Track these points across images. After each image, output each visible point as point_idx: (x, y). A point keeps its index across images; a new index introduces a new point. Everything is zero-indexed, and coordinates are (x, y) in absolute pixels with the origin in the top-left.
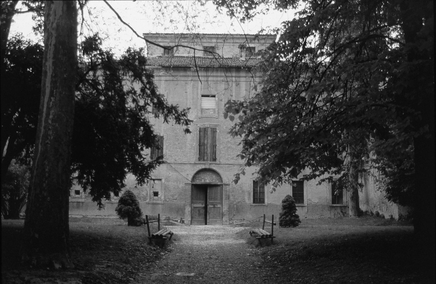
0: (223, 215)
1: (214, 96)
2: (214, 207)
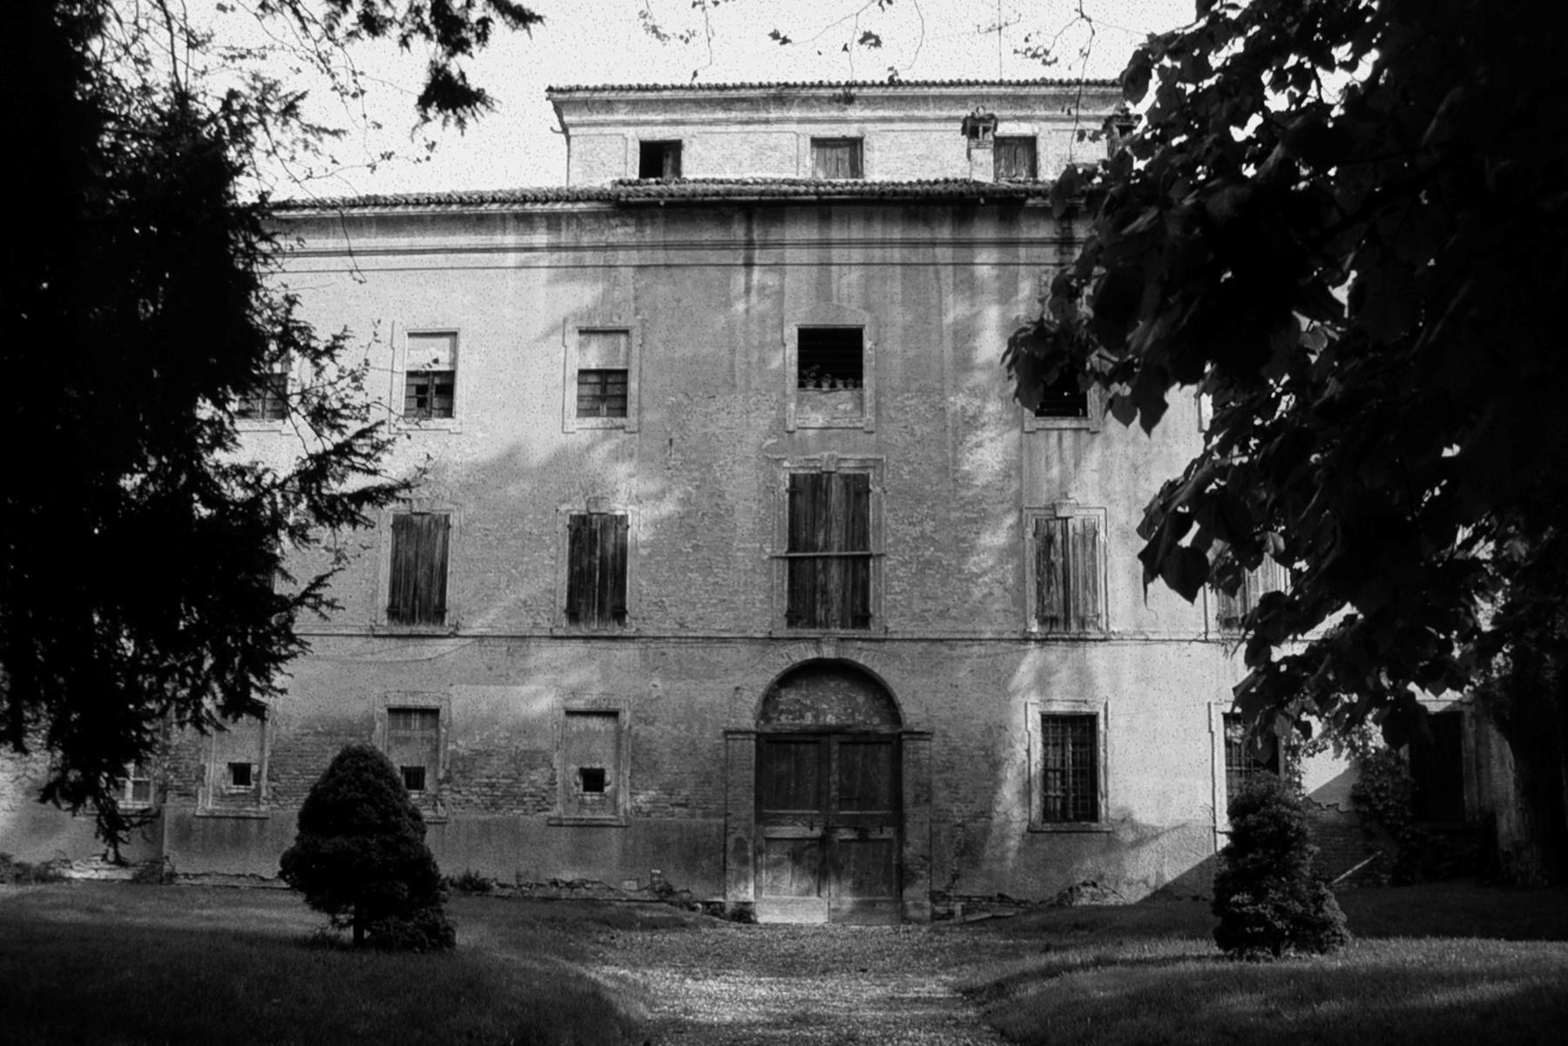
0: (902, 877)
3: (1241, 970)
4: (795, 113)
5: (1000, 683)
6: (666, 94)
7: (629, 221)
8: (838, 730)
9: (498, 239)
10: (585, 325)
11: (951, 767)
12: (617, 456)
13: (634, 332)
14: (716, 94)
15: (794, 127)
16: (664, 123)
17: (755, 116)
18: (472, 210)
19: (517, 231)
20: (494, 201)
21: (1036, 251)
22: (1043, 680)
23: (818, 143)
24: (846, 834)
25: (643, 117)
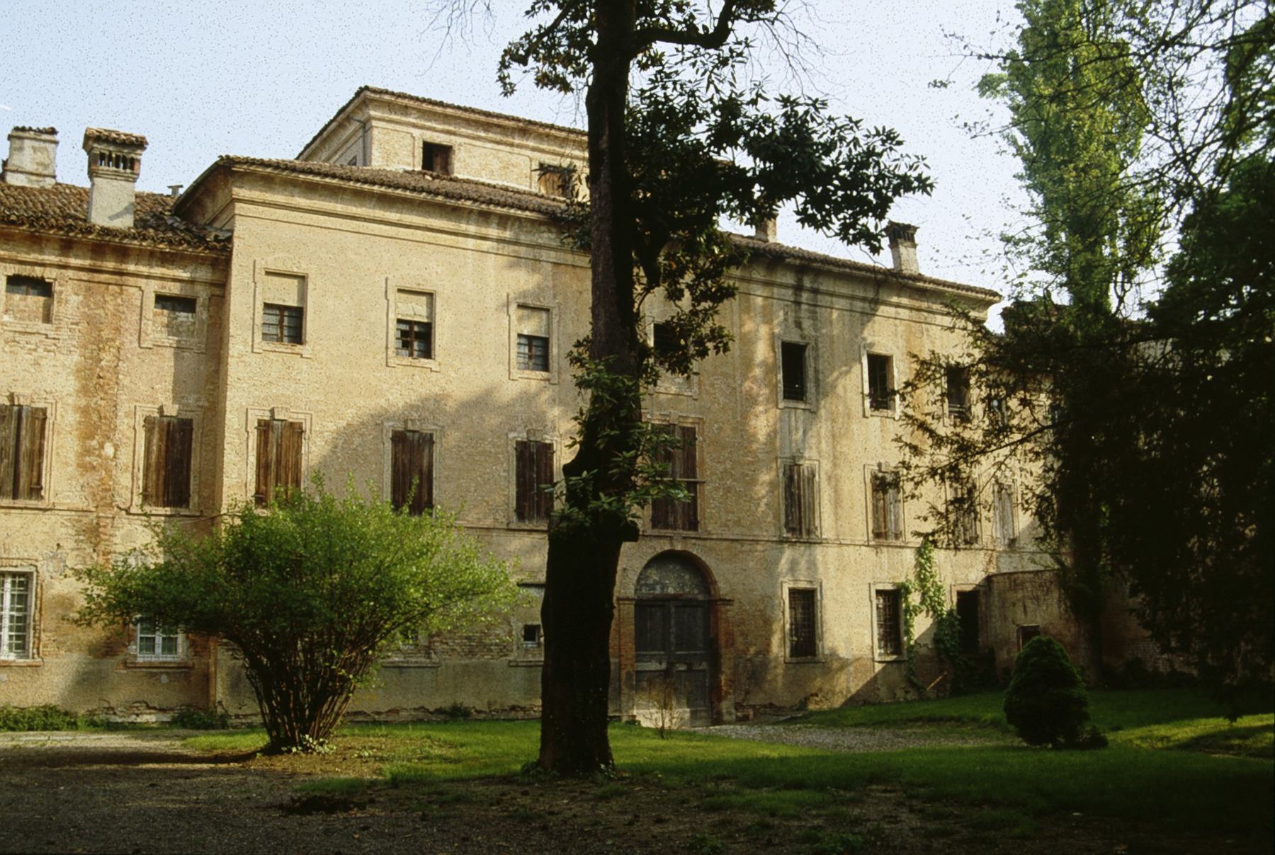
3: (1233, 718)
4: (531, 143)
5: (770, 567)
6: (449, 111)
7: (553, 230)
8: (675, 598)
9: (463, 227)
10: (521, 301)
11: (743, 622)
12: (553, 401)
13: (555, 311)
14: (483, 118)
15: (528, 153)
16: (443, 131)
17: (505, 139)
18: (453, 202)
19: (478, 224)
21: (783, 291)
22: (793, 567)
23: (544, 169)
24: (683, 668)
25: (428, 124)
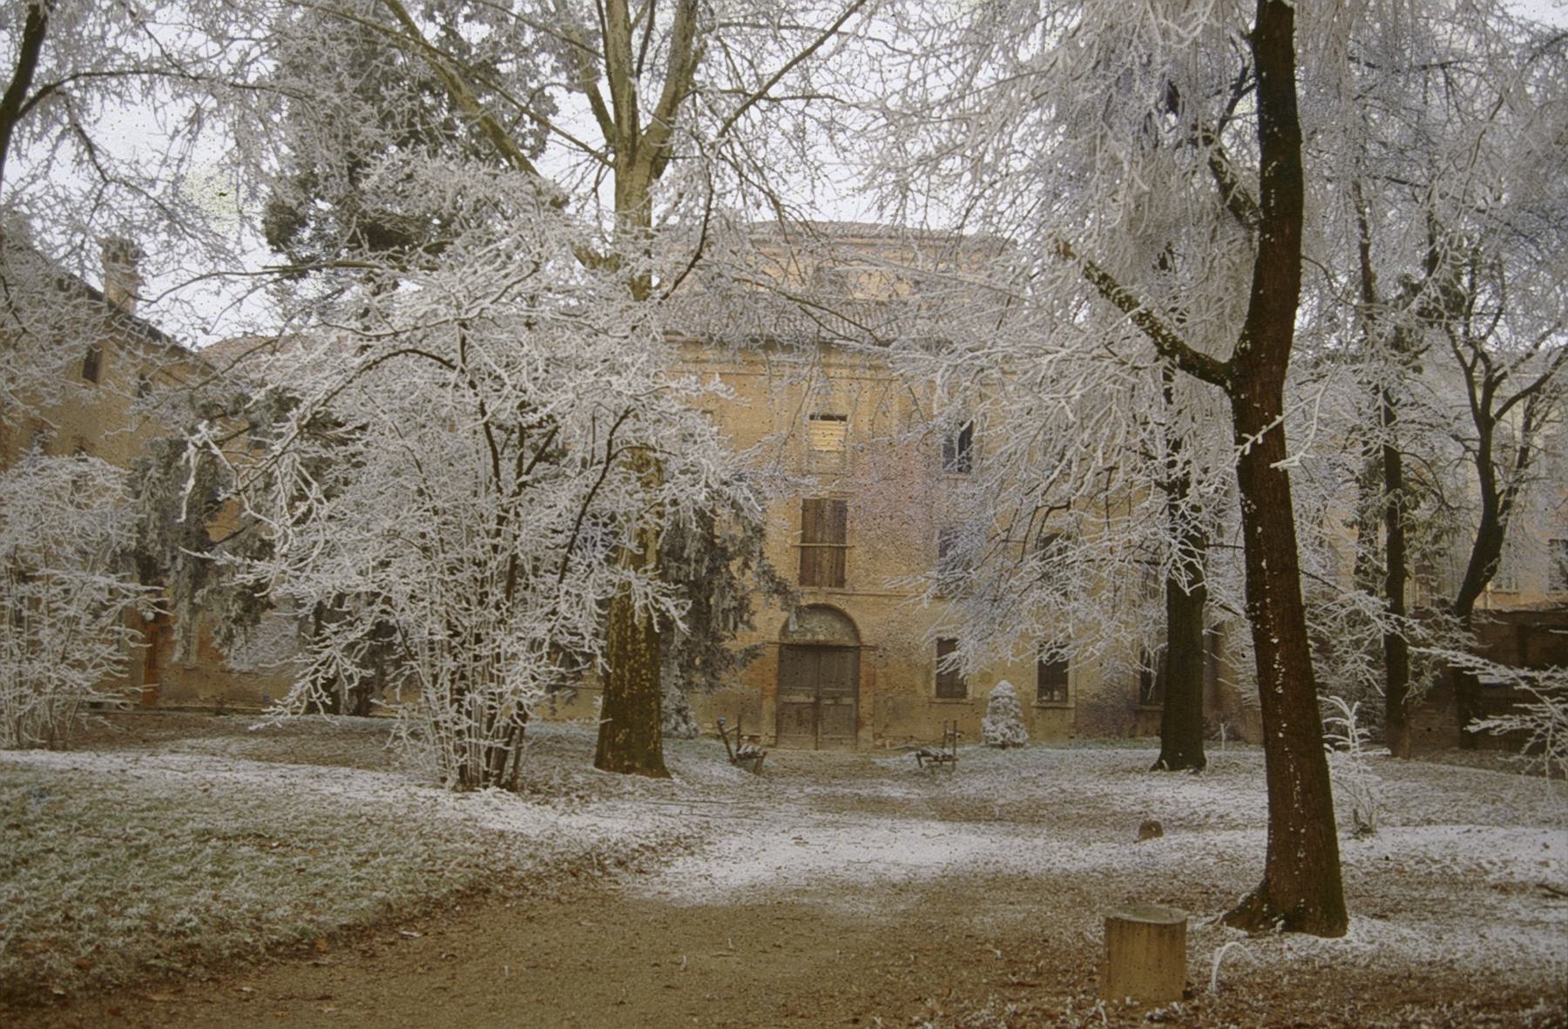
0: (858, 724)
1: (843, 418)
2: (836, 704)
20: (1254, 377)
